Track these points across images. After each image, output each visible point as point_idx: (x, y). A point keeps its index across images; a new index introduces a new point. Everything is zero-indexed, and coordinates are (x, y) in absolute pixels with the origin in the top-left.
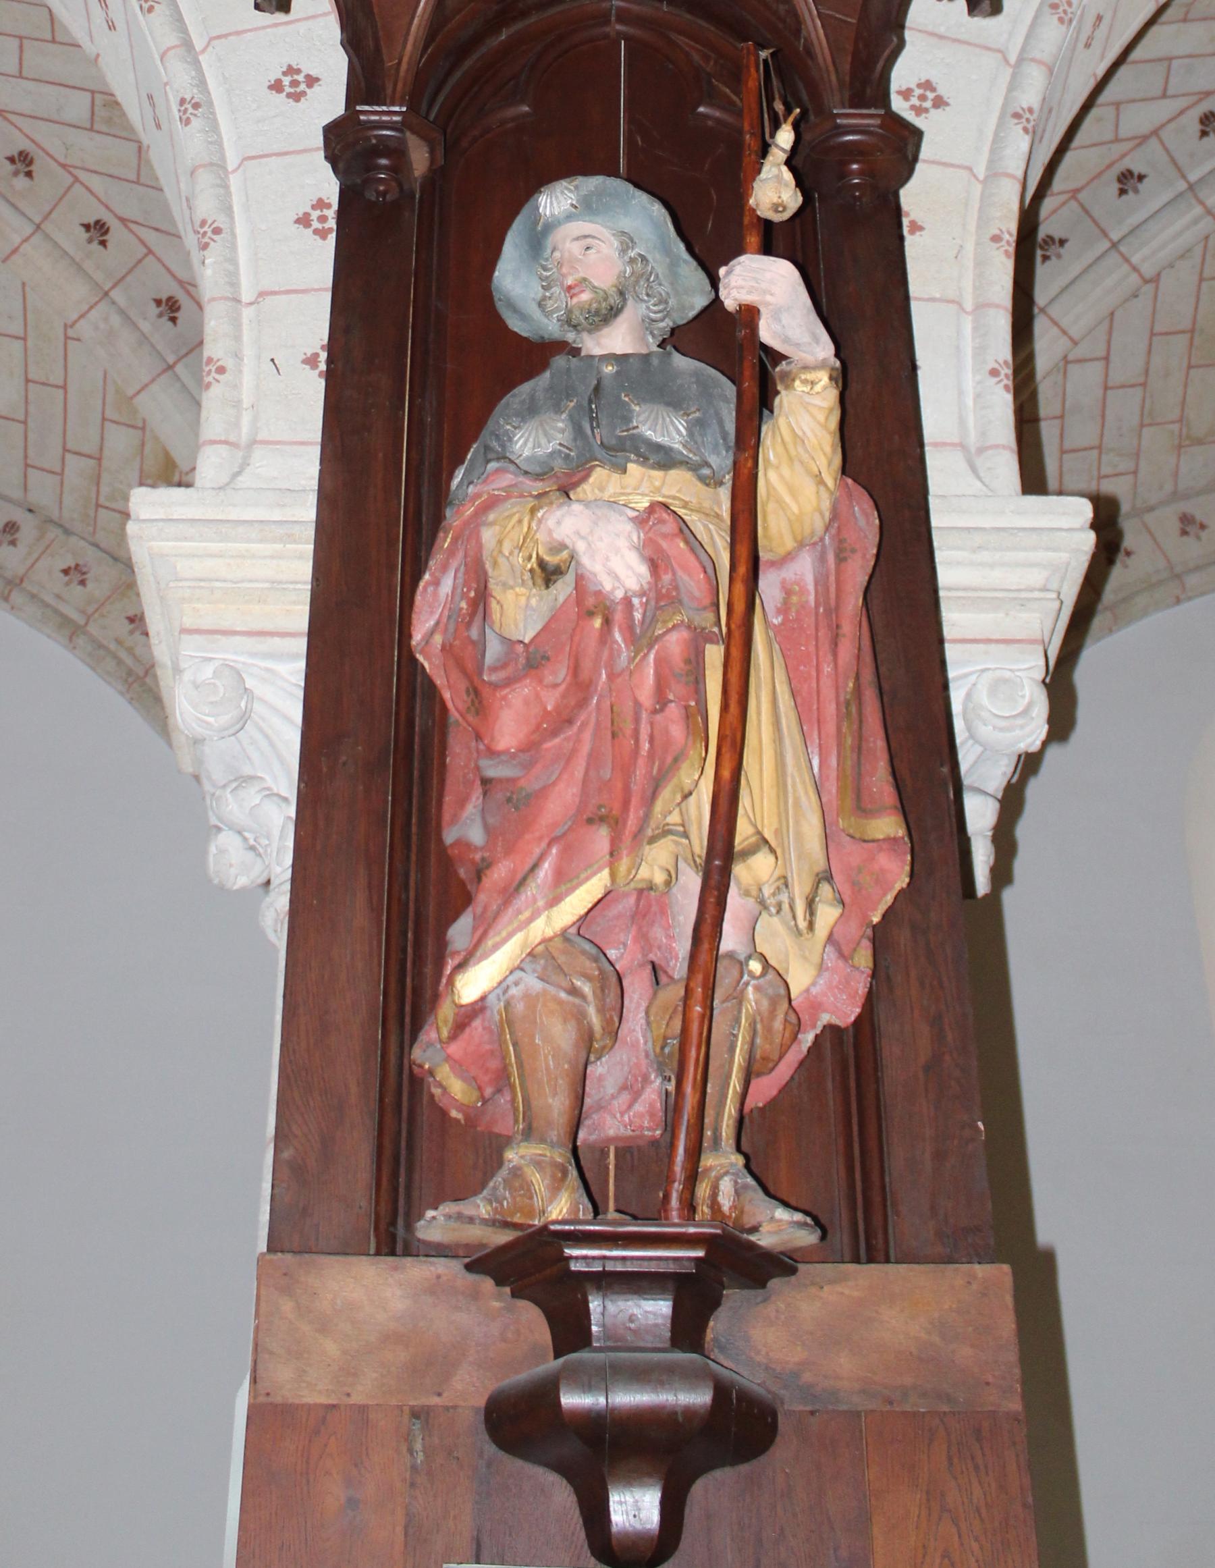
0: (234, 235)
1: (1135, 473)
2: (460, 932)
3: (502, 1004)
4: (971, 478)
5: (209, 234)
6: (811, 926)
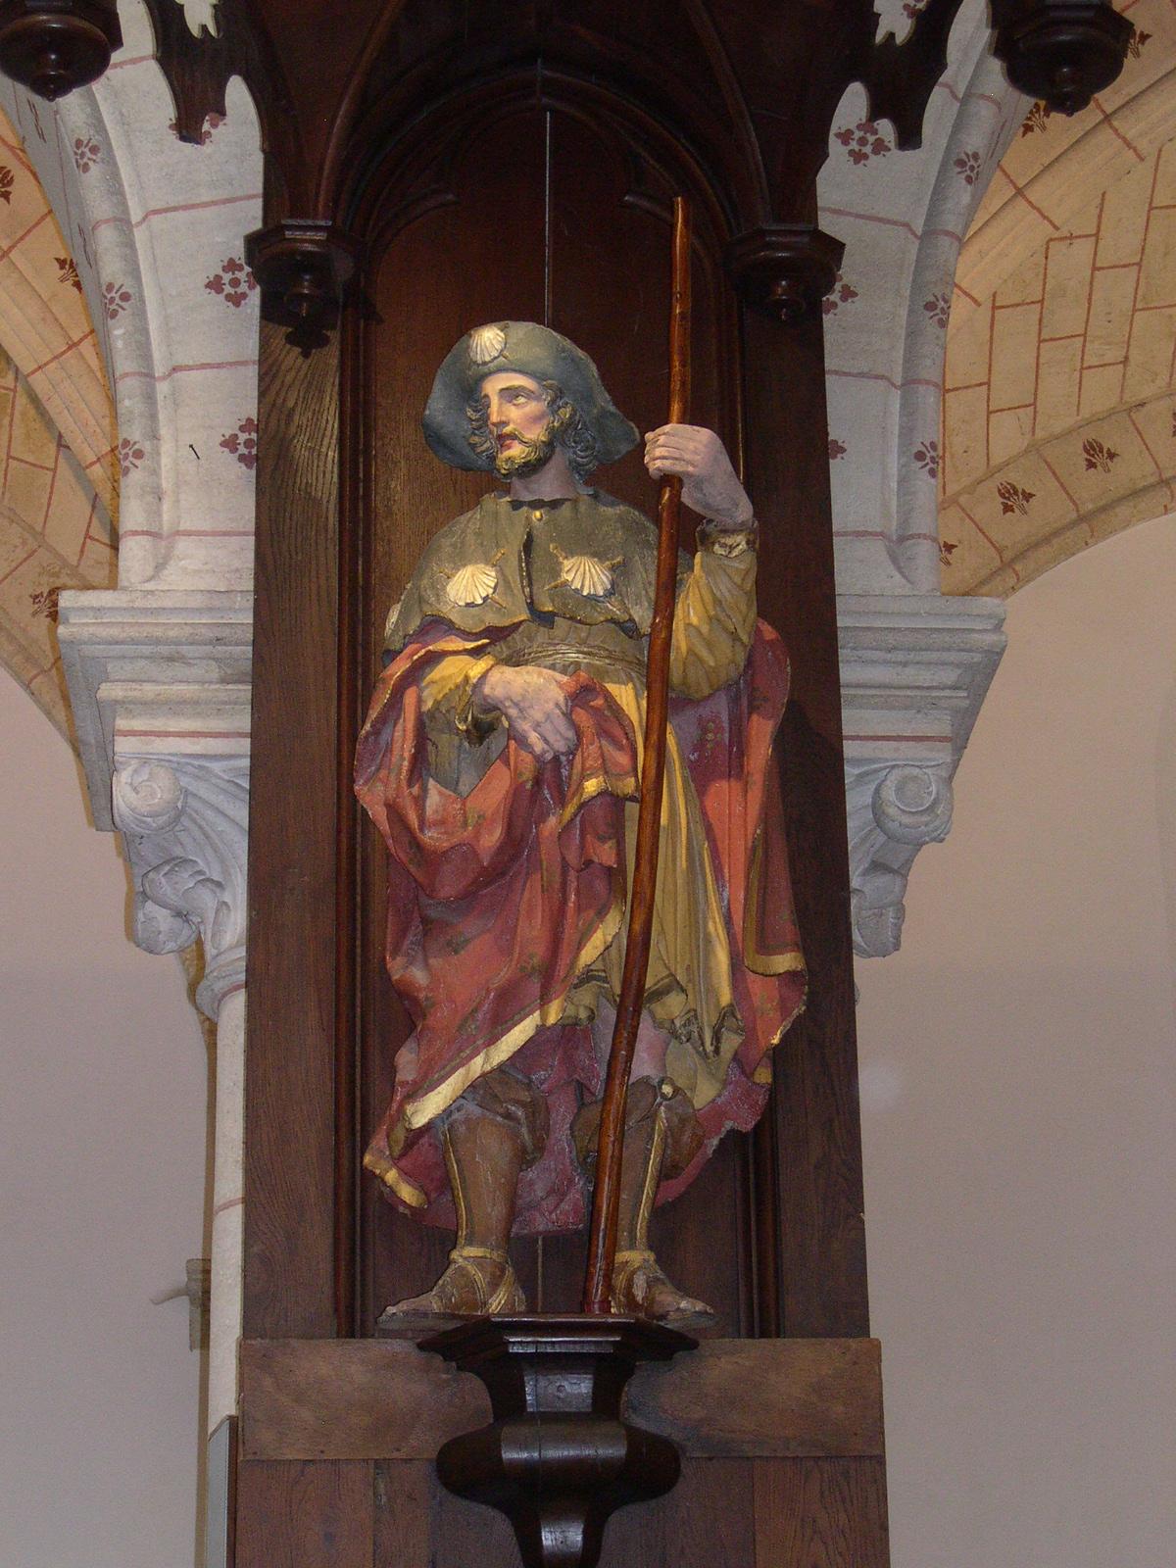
0: (142, 300)
1: (1126, 361)
2: (407, 1062)
3: (446, 1126)
4: (891, 569)
5: (117, 301)
6: (717, 1051)
